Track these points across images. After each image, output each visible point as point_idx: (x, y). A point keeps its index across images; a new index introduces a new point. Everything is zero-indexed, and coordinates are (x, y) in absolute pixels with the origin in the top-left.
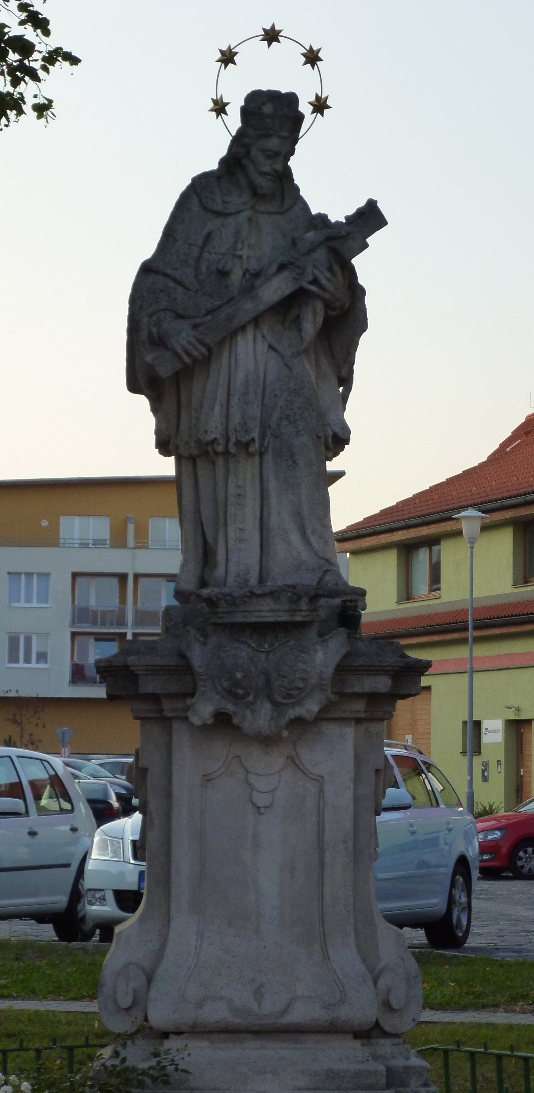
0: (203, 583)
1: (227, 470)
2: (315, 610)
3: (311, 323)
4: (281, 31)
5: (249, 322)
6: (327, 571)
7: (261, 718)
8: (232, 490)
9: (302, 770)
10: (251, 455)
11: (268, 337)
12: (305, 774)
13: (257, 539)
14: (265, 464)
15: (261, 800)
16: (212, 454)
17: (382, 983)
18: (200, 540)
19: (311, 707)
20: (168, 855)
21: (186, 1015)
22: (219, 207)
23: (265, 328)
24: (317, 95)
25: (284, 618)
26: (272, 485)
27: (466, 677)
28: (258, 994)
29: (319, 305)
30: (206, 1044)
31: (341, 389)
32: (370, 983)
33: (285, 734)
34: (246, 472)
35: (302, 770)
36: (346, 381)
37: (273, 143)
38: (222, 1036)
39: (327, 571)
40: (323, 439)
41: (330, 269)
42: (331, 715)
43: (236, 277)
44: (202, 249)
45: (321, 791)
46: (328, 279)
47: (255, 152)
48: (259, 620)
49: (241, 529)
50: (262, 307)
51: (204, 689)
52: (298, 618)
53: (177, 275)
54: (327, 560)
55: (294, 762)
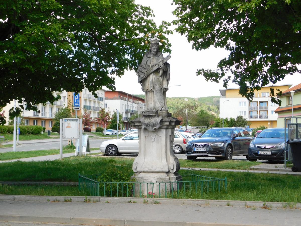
22: (148, 57)
43: (151, 66)
47: (152, 49)
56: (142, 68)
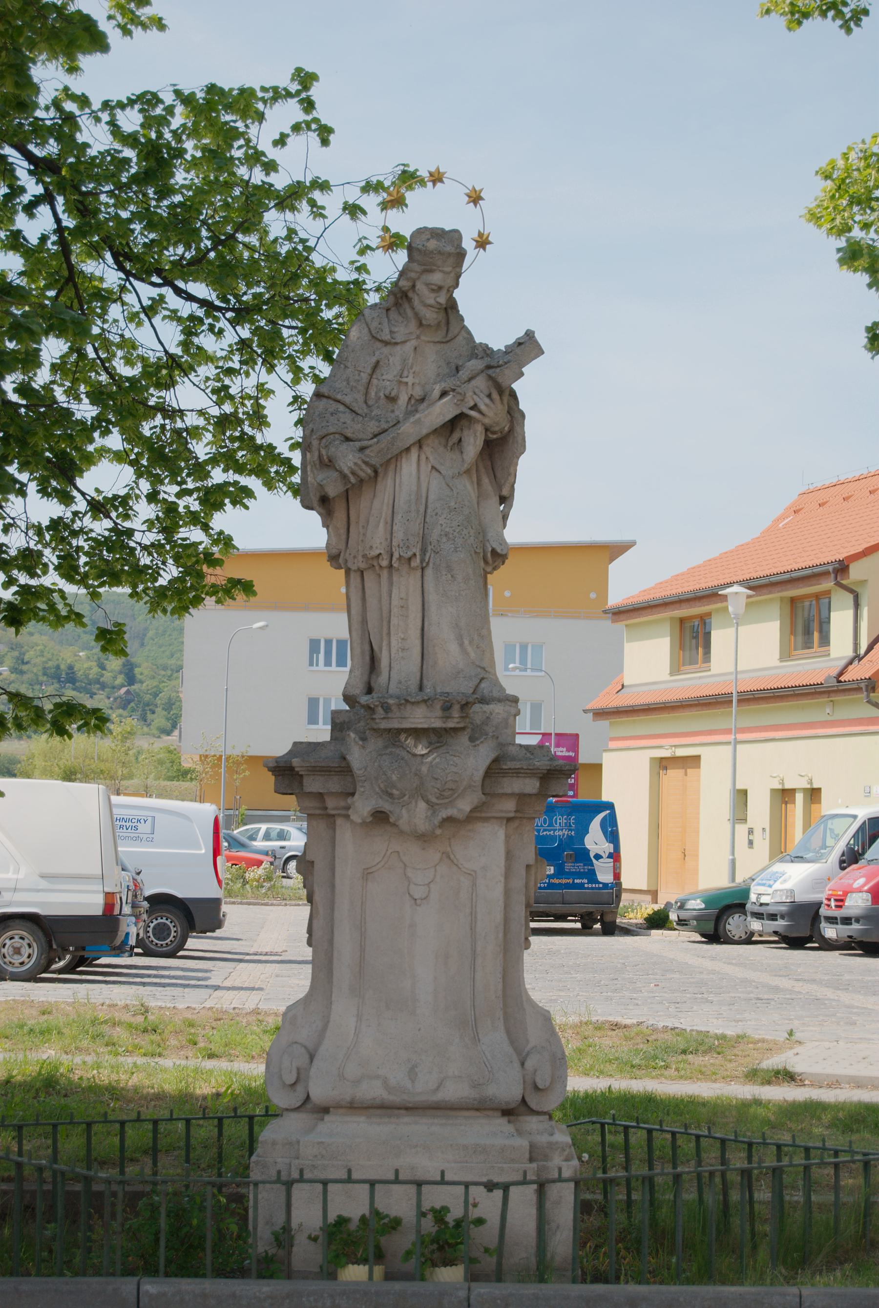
0: (369, 690)
1: (391, 583)
2: (467, 717)
3: (473, 443)
4: (445, 173)
5: (414, 444)
6: (483, 679)
7: (417, 816)
8: (395, 602)
9: (457, 865)
10: (415, 569)
11: (431, 458)
12: (460, 868)
13: (418, 649)
14: (425, 578)
15: (418, 892)
16: (377, 568)
17: (529, 1064)
18: (367, 647)
19: (465, 805)
20: (331, 942)
21: (346, 1093)
22: (386, 336)
23: (427, 450)
24: (479, 232)
25: (438, 724)
26: (432, 597)
27: (730, 748)
28: (412, 1073)
29: (480, 429)
30: (362, 1119)
31: (502, 508)
32: (517, 1065)
33: (438, 832)
34: (406, 585)
35: (457, 865)
36: (506, 499)
37: (436, 278)
38: (379, 1112)
39: (483, 679)
40: (482, 555)
41: (489, 396)
42: (478, 815)
43: (403, 399)
44: (371, 376)
45: (474, 885)
46: (486, 405)
47: (419, 286)
48: (413, 726)
49: (403, 639)
50: (425, 431)
51: (362, 789)
52: (451, 724)
53: (348, 400)
54: (484, 669)
55: (449, 857)
56: (341, 408)
